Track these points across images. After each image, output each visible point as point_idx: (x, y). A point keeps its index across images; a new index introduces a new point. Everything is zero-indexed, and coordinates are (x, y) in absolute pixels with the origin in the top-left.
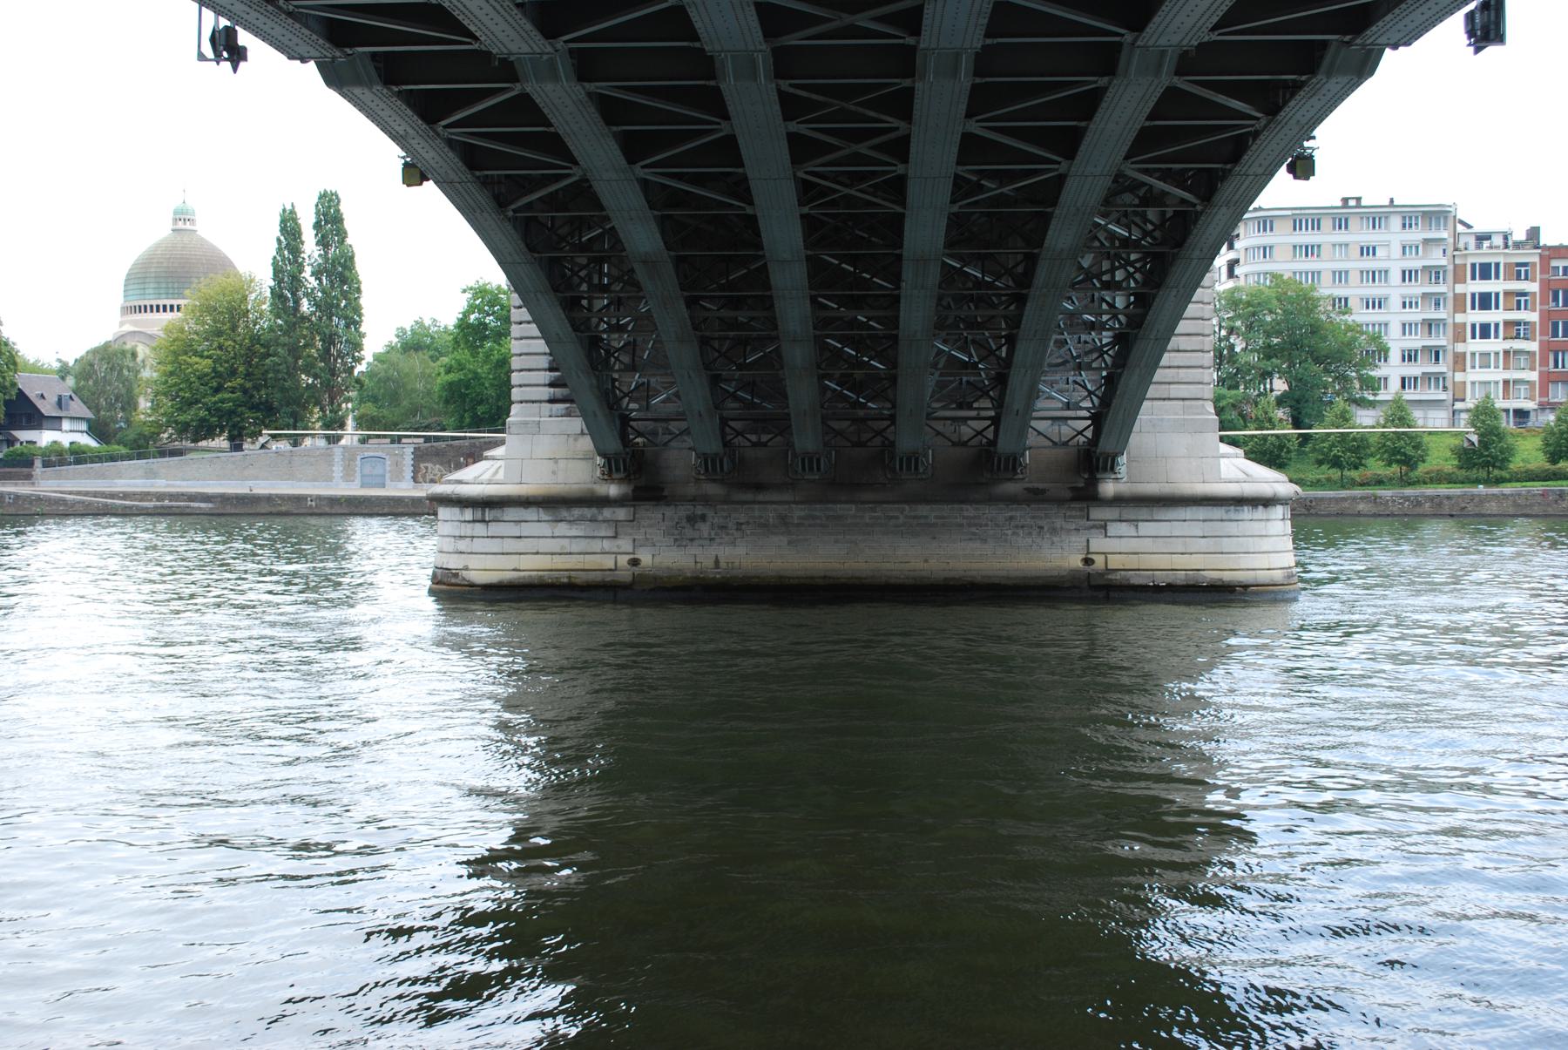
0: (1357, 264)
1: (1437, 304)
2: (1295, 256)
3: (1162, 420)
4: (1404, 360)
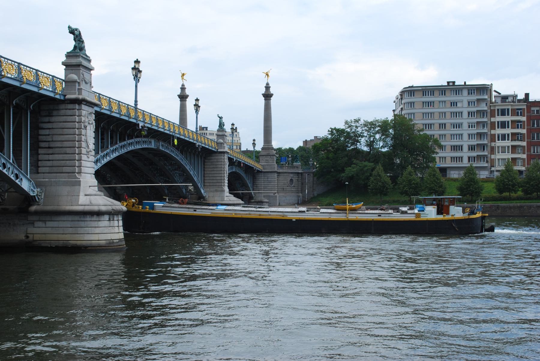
0: (449, 110)
1: (484, 127)
2: (423, 106)
3: (59, 181)
4: (469, 150)
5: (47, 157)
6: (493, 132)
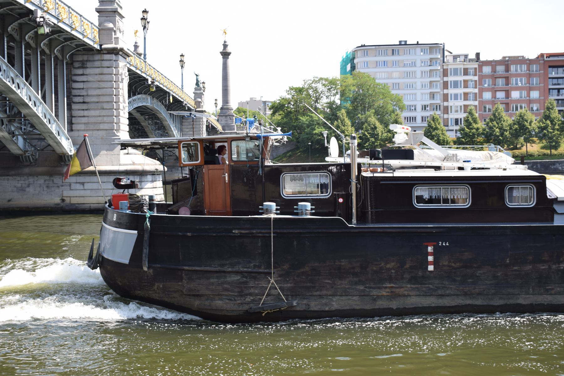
5: (81, 113)
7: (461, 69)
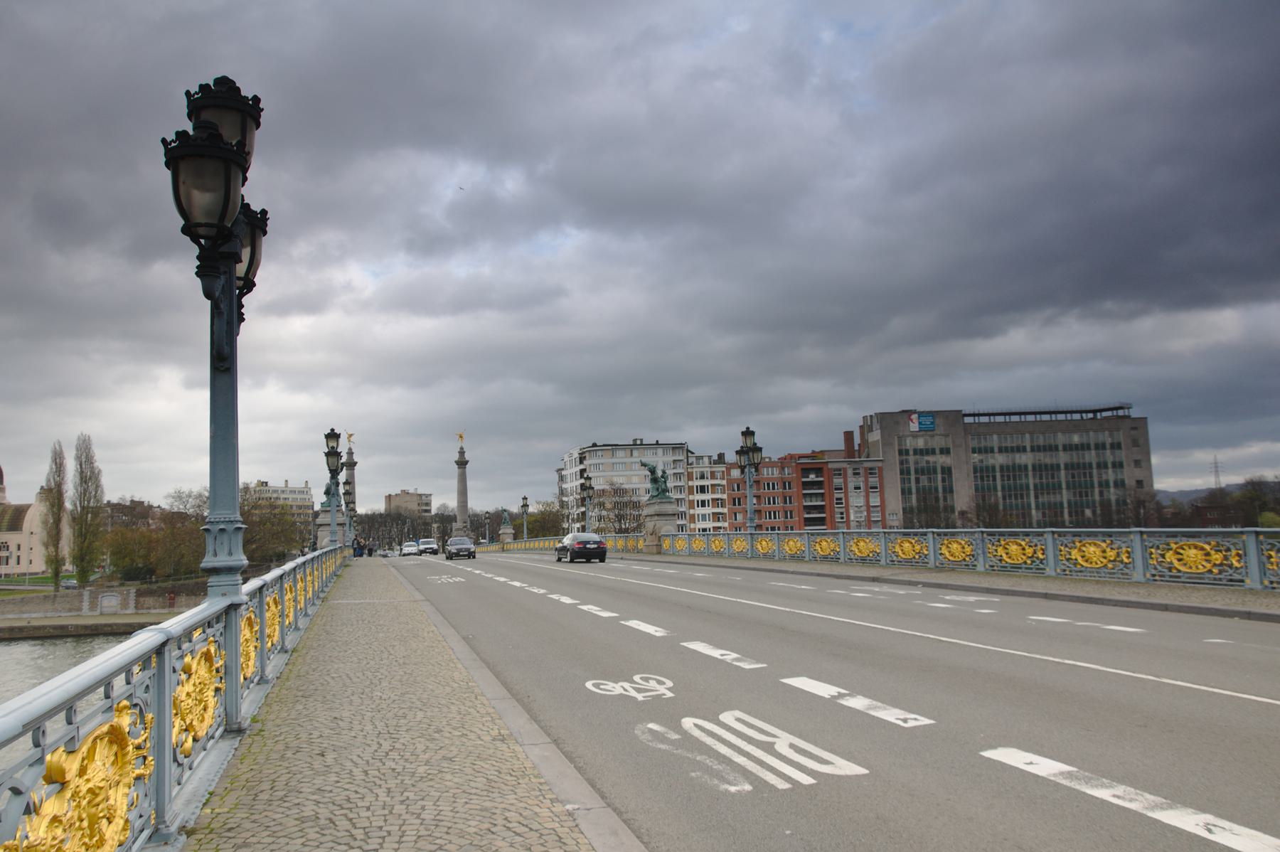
6: (691, 497)
7: (707, 472)
